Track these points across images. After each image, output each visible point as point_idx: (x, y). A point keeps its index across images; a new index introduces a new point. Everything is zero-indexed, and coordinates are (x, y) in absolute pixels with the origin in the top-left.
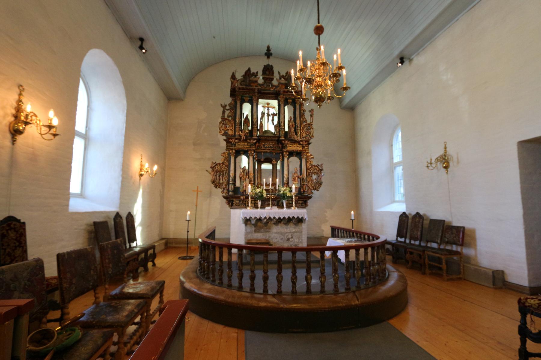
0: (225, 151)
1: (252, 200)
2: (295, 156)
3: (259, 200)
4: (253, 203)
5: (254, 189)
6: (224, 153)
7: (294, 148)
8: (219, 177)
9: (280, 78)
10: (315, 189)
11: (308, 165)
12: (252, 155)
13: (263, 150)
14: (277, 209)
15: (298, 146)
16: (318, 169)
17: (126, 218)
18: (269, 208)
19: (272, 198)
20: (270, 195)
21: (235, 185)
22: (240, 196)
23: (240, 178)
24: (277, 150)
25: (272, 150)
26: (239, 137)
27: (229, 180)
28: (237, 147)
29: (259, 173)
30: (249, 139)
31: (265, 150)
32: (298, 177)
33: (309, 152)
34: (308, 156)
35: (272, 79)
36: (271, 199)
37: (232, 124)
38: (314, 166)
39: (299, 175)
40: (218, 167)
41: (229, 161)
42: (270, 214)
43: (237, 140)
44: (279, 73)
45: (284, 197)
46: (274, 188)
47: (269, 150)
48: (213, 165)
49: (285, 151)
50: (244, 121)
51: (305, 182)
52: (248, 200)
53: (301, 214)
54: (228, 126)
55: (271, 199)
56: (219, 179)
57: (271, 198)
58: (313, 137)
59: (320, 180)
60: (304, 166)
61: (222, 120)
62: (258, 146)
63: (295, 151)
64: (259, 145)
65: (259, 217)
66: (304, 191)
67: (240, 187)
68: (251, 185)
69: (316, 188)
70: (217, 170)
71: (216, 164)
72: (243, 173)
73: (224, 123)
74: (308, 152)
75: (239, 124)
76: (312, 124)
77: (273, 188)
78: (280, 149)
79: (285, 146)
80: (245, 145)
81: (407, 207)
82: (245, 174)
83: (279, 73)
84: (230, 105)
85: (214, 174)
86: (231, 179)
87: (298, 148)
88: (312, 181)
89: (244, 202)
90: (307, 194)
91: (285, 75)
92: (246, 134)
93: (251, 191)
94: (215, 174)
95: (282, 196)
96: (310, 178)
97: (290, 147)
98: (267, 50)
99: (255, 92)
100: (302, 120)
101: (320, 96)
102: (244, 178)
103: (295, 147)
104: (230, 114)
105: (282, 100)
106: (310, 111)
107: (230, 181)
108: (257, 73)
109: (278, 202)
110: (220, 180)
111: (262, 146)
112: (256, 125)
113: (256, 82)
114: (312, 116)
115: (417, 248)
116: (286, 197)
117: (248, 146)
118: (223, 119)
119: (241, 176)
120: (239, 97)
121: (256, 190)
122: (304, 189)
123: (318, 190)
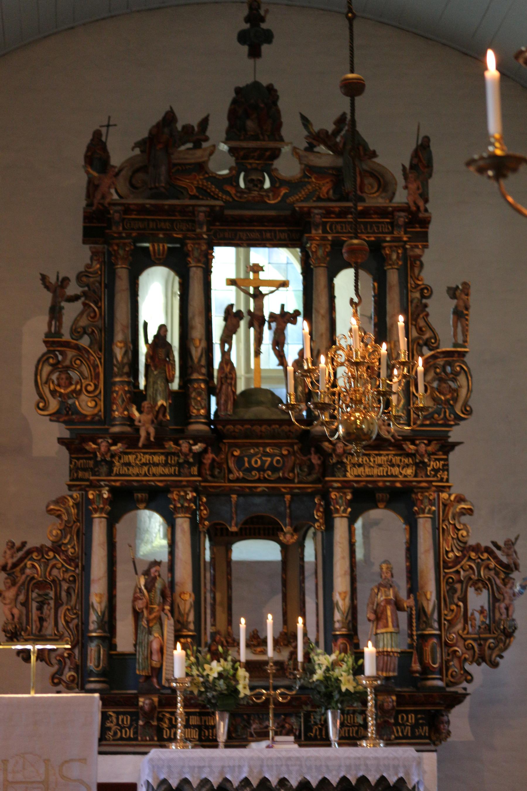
0: (66, 492)
1: (188, 714)
2: (386, 507)
3: (222, 711)
4: (195, 726)
5: (198, 663)
6: (61, 501)
7: (376, 471)
8: (40, 608)
9: (310, 148)
10: (480, 659)
11: (445, 546)
12: (187, 510)
13: (238, 480)
14: (296, 746)
15: (397, 460)
16: (493, 564)
18: (264, 744)
19: (277, 704)
20: (267, 689)
21: (113, 646)
22: (136, 697)
23: (137, 615)
24: (299, 482)
25: (280, 480)
26: (128, 429)
27: (85, 622)
28: (116, 475)
29: (222, 584)
30: (170, 440)
31: (244, 480)
32: (398, 606)
33: (449, 487)
34: (445, 505)
35: (275, 154)
36: (272, 706)
37: (96, 367)
38: (477, 548)
39: (403, 594)
40: (34, 566)
42: (265, 769)
43: (119, 445)
44: (306, 122)
45: (329, 696)
46: (290, 659)
47: (265, 480)
48: (12, 557)
49: (336, 485)
50: (147, 356)
51: (432, 627)
52: (173, 714)
53: (396, 768)
54: (74, 375)
55: (272, 706)
56: (41, 620)
57: (271, 700)
58: (470, 413)
59: (504, 616)
60: (427, 551)
61: (49, 352)
62: (212, 466)
63: (380, 484)
65: (220, 780)
66: (426, 670)
67: (133, 655)
68: (184, 648)
69: (487, 652)
70: (33, 578)
71: (25, 549)
72: (149, 591)
73: (59, 362)
74: (444, 487)
75: (126, 369)
76: (463, 354)
77: (284, 656)
78: (314, 476)
79: (335, 465)
82: (158, 598)
84: (84, 279)
85: (17, 595)
86: (93, 617)
87: (396, 471)
88: (466, 622)
89: (155, 723)
90: (439, 683)
91: (330, 128)
92: (156, 417)
93: (184, 670)
94: (22, 598)
95: (319, 692)
96: (454, 607)
97: (360, 465)
98: (247, 20)
99: (193, 221)
101: (357, 429)
102: (152, 616)
103: (380, 465)
104: (84, 322)
105: (320, 253)
106: (453, 292)
107: (92, 627)
108: (204, 123)
109: (307, 716)
110: (45, 624)
111: (232, 465)
112: (204, 370)
115: (30, 597)
116: (337, 696)
117: (166, 471)
119: (140, 605)
120: (125, 244)
121: (206, 666)
122: (428, 660)
123: (495, 665)
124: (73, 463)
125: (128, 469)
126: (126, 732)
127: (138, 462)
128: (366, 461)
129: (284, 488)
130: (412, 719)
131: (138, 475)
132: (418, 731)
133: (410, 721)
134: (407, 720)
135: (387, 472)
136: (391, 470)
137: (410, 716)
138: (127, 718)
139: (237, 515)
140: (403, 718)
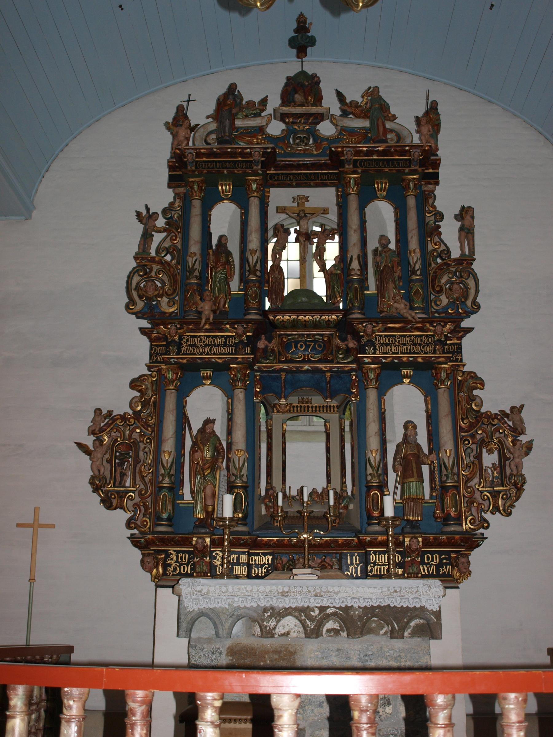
9: (345, 114)
28: (184, 354)
44: (340, 96)
49: (367, 361)
61: (138, 266)
63: (405, 359)
83: (340, 96)
94: (108, 456)
97: (387, 345)
98: (296, 31)
100: (430, 247)
103: (404, 345)
104: (167, 244)
108: (264, 102)
113: (261, 130)
117: (225, 350)
124: (154, 349)
125: (194, 350)
126: (184, 568)
127: (201, 344)
128: (392, 341)
129: (325, 367)
130: (436, 559)
131: (201, 354)
132: (443, 570)
133: (435, 561)
134: (432, 560)
135: (410, 350)
136: (413, 348)
137: (434, 556)
138: (185, 556)
139: (285, 389)
140: (428, 557)
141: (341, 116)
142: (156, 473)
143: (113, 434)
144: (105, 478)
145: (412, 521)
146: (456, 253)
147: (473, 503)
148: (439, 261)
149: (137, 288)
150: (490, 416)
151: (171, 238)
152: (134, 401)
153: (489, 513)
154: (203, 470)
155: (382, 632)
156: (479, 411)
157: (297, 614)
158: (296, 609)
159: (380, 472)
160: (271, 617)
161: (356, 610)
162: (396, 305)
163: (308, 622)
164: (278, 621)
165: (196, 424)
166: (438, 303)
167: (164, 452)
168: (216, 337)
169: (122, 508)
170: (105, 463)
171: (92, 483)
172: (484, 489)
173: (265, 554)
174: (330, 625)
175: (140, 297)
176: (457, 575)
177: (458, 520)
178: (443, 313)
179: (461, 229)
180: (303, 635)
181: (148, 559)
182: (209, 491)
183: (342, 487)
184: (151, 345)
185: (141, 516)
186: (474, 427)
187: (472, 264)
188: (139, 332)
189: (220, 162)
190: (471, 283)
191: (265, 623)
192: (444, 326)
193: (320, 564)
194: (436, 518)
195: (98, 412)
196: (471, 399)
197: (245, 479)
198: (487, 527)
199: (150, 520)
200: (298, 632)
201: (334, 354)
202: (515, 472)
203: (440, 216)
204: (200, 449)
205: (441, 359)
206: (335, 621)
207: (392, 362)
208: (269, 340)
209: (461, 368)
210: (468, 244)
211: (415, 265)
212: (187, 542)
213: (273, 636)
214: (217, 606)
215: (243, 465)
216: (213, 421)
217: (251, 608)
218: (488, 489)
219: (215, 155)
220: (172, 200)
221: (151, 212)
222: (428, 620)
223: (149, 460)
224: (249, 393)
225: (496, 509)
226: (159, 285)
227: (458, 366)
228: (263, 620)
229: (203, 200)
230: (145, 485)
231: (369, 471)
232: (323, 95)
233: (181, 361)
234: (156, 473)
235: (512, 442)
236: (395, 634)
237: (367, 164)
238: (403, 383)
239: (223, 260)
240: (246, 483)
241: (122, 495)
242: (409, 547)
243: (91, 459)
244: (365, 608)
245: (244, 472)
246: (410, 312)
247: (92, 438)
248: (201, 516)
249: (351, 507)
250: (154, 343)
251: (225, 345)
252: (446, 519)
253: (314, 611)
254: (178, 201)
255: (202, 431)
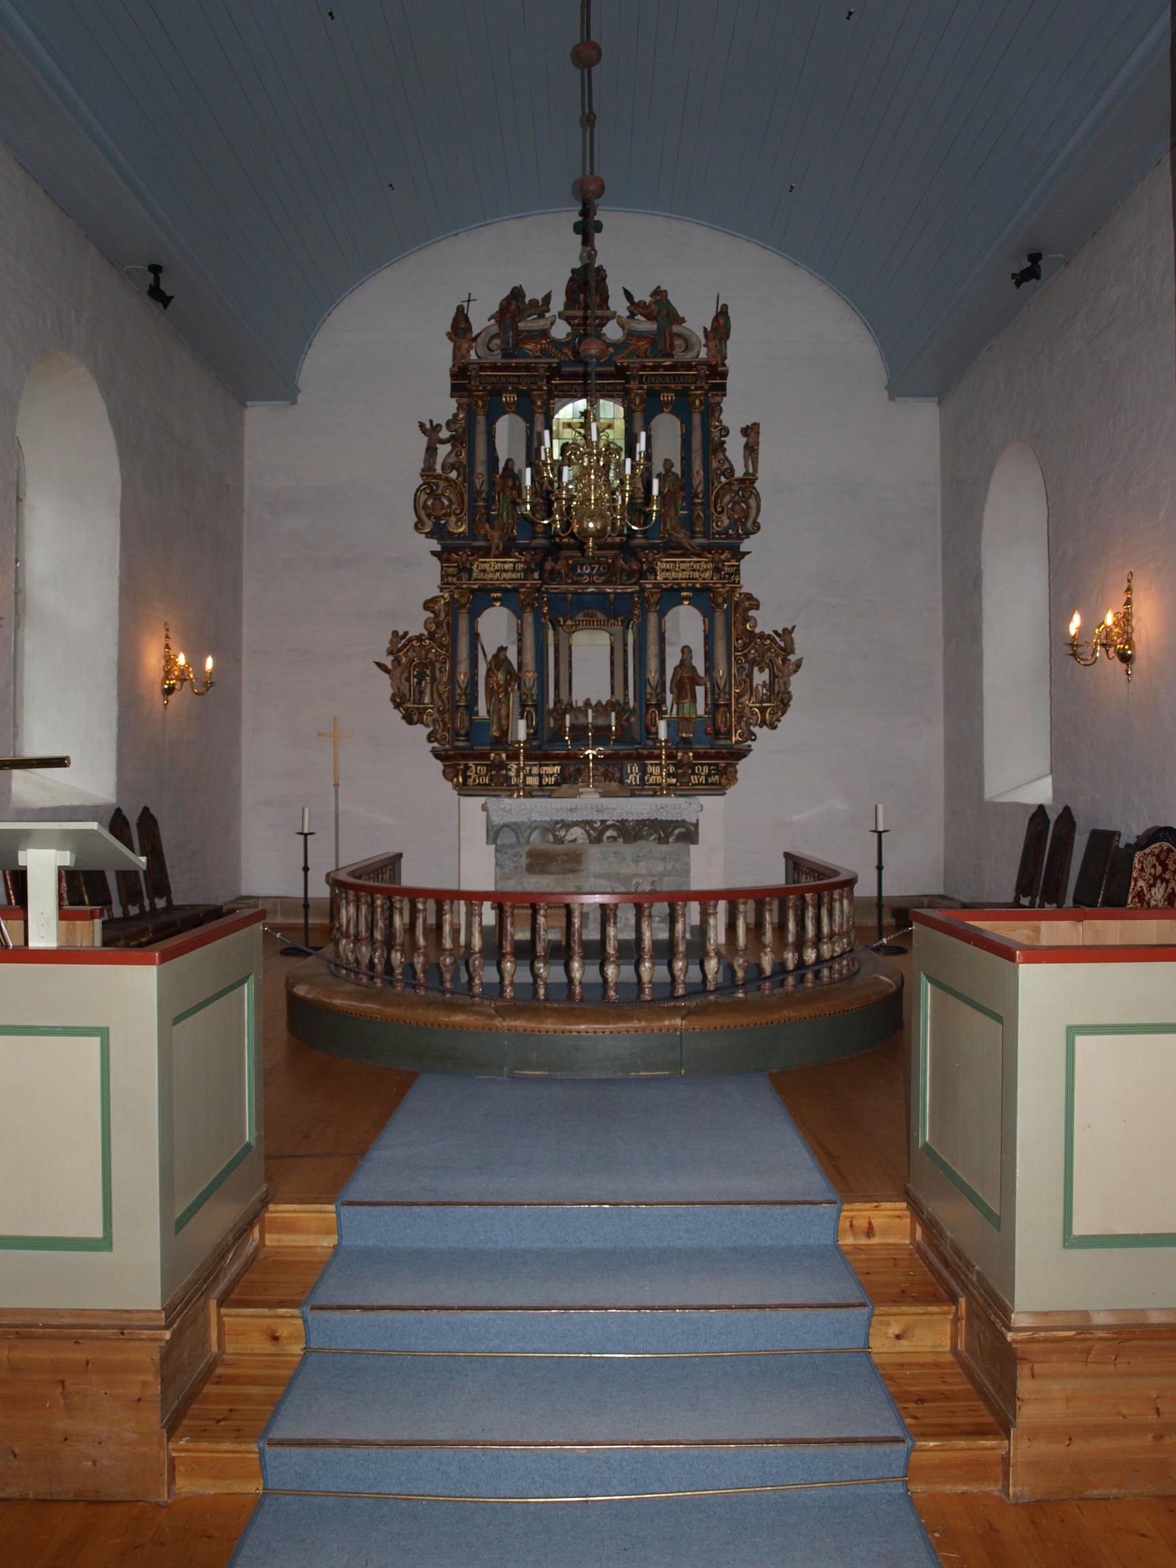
6: (434, 600)
9: (632, 316)
17: (139, 825)
28: (475, 580)
41: (453, 629)
49: (648, 586)
63: (684, 585)
64: (558, 567)
80: (506, 571)
81: (1056, 790)
85: (402, 673)
94: (406, 675)
100: (715, 464)
103: (684, 570)
104: (452, 460)
108: (547, 298)
113: (545, 333)
114: (751, 450)
118: (428, 476)
123: (773, 727)
130: (706, 770)
131: (491, 580)
134: (702, 771)
141: (628, 317)
142: (452, 693)
143: (410, 654)
144: (404, 695)
145: (685, 738)
146: (739, 473)
147: (743, 717)
148: (723, 479)
149: (425, 507)
150: (762, 636)
151: (456, 453)
152: (429, 621)
153: (757, 727)
154: (498, 694)
155: (652, 838)
156: (753, 632)
157: (582, 825)
158: (583, 822)
159: (658, 691)
160: (561, 828)
161: (630, 821)
162: (676, 535)
163: (592, 832)
164: (567, 831)
165: (491, 651)
166: (719, 524)
167: (460, 673)
168: (505, 562)
169: (422, 723)
170: (404, 682)
171: (393, 700)
172: (753, 705)
173: (554, 765)
174: (609, 833)
175: (429, 516)
176: (724, 781)
177: (728, 734)
178: (724, 534)
179: (746, 446)
180: (588, 841)
181: (448, 770)
182: (503, 713)
183: (625, 699)
184: (442, 566)
185: (440, 730)
186: (747, 647)
187: (754, 483)
188: (430, 554)
189: (504, 376)
190: (752, 502)
191: (557, 833)
192: (722, 554)
193: (603, 772)
194: (707, 734)
195: (395, 634)
196: (746, 619)
197: (535, 698)
198: (754, 740)
199: (449, 733)
200: (584, 839)
201: (618, 576)
202: (783, 689)
203: (725, 431)
204: (494, 673)
205: (718, 585)
206: (613, 830)
207: (672, 587)
208: (556, 561)
209: (738, 590)
210: (752, 463)
211: (697, 487)
212: (485, 756)
213: (563, 842)
214: (519, 820)
215: (533, 685)
216: (506, 649)
217: (545, 821)
218: (757, 705)
219: (499, 369)
220: (456, 412)
221: (434, 424)
222: (688, 830)
223: (445, 679)
224: (537, 614)
225: (763, 723)
226: (446, 503)
227: (736, 588)
228: (555, 831)
229: (486, 415)
230: (442, 701)
231: (649, 690)
232: (610, 293)
233: (472, 586)
234: (452, 693)
235: (782, 661)
236: (662, 841)
237: (653, 379)
238: (682, 604)
239: (510, 484)
240: (536, 701)
241: (422, 712)
242: (681, 761)
243: (391, 678)
244: (637, 821)
245: (534, 691)
246: (690, 541)
247: (391, 658)
248: (496, 734)
249: (632, 719)
250: (444, 565)
251: (514, 570)
252: (717, 733)
253: (596, 823)
254: (461, 412)
255: (495, 656)
